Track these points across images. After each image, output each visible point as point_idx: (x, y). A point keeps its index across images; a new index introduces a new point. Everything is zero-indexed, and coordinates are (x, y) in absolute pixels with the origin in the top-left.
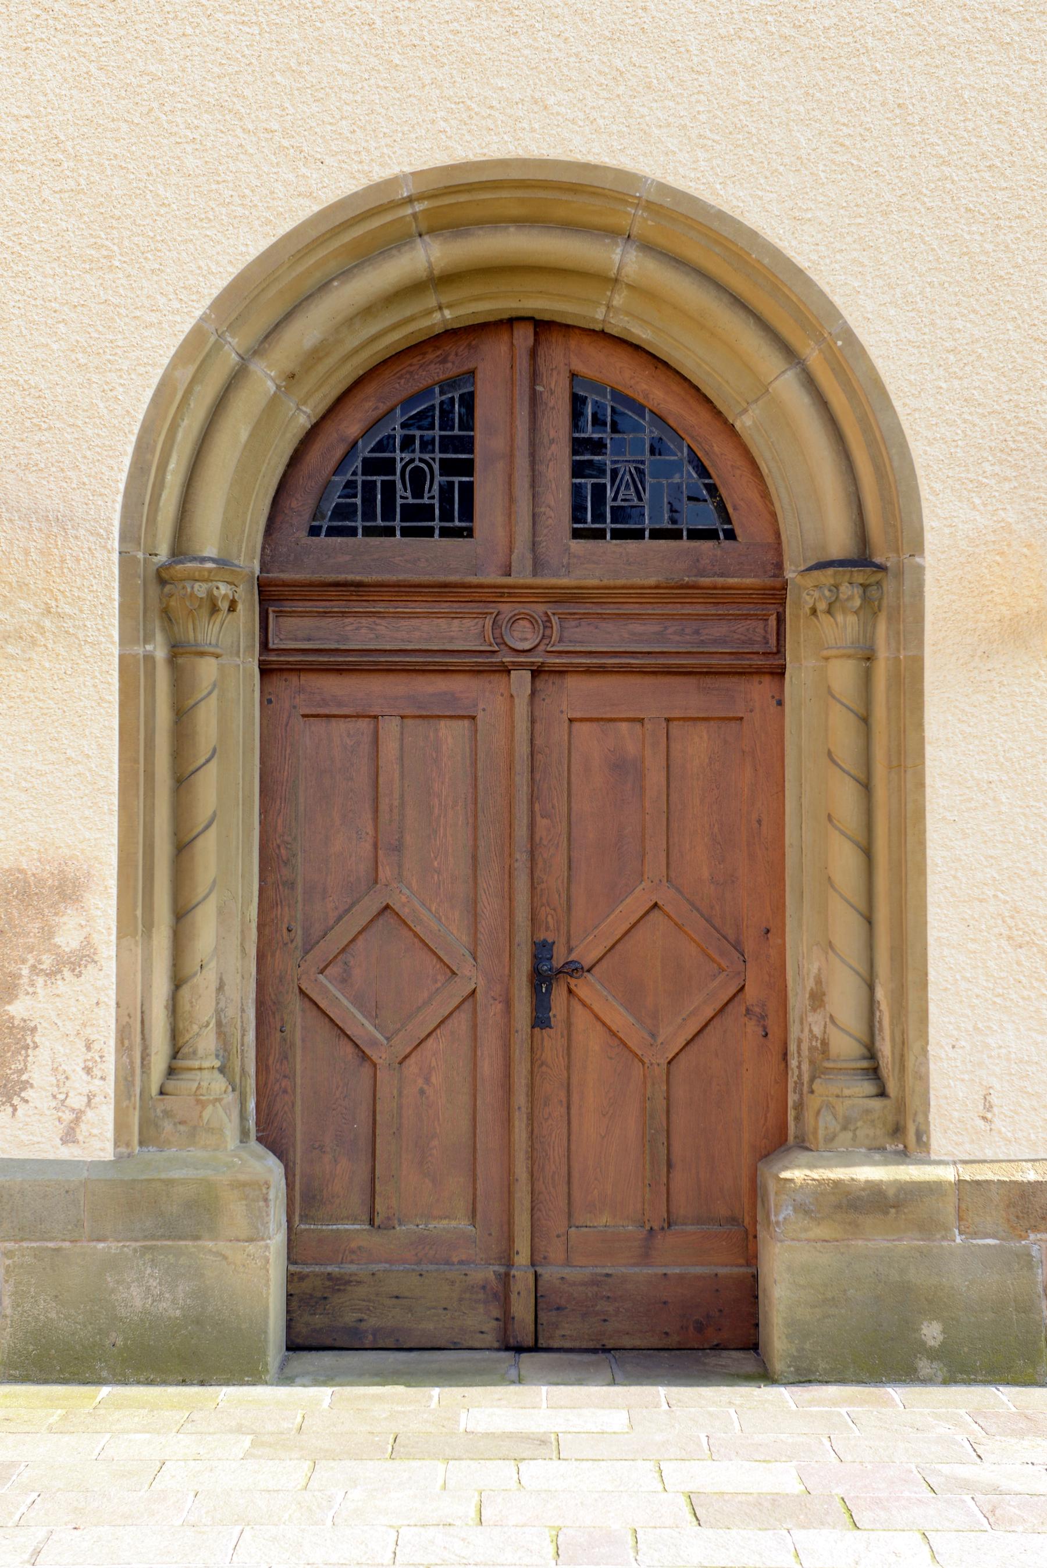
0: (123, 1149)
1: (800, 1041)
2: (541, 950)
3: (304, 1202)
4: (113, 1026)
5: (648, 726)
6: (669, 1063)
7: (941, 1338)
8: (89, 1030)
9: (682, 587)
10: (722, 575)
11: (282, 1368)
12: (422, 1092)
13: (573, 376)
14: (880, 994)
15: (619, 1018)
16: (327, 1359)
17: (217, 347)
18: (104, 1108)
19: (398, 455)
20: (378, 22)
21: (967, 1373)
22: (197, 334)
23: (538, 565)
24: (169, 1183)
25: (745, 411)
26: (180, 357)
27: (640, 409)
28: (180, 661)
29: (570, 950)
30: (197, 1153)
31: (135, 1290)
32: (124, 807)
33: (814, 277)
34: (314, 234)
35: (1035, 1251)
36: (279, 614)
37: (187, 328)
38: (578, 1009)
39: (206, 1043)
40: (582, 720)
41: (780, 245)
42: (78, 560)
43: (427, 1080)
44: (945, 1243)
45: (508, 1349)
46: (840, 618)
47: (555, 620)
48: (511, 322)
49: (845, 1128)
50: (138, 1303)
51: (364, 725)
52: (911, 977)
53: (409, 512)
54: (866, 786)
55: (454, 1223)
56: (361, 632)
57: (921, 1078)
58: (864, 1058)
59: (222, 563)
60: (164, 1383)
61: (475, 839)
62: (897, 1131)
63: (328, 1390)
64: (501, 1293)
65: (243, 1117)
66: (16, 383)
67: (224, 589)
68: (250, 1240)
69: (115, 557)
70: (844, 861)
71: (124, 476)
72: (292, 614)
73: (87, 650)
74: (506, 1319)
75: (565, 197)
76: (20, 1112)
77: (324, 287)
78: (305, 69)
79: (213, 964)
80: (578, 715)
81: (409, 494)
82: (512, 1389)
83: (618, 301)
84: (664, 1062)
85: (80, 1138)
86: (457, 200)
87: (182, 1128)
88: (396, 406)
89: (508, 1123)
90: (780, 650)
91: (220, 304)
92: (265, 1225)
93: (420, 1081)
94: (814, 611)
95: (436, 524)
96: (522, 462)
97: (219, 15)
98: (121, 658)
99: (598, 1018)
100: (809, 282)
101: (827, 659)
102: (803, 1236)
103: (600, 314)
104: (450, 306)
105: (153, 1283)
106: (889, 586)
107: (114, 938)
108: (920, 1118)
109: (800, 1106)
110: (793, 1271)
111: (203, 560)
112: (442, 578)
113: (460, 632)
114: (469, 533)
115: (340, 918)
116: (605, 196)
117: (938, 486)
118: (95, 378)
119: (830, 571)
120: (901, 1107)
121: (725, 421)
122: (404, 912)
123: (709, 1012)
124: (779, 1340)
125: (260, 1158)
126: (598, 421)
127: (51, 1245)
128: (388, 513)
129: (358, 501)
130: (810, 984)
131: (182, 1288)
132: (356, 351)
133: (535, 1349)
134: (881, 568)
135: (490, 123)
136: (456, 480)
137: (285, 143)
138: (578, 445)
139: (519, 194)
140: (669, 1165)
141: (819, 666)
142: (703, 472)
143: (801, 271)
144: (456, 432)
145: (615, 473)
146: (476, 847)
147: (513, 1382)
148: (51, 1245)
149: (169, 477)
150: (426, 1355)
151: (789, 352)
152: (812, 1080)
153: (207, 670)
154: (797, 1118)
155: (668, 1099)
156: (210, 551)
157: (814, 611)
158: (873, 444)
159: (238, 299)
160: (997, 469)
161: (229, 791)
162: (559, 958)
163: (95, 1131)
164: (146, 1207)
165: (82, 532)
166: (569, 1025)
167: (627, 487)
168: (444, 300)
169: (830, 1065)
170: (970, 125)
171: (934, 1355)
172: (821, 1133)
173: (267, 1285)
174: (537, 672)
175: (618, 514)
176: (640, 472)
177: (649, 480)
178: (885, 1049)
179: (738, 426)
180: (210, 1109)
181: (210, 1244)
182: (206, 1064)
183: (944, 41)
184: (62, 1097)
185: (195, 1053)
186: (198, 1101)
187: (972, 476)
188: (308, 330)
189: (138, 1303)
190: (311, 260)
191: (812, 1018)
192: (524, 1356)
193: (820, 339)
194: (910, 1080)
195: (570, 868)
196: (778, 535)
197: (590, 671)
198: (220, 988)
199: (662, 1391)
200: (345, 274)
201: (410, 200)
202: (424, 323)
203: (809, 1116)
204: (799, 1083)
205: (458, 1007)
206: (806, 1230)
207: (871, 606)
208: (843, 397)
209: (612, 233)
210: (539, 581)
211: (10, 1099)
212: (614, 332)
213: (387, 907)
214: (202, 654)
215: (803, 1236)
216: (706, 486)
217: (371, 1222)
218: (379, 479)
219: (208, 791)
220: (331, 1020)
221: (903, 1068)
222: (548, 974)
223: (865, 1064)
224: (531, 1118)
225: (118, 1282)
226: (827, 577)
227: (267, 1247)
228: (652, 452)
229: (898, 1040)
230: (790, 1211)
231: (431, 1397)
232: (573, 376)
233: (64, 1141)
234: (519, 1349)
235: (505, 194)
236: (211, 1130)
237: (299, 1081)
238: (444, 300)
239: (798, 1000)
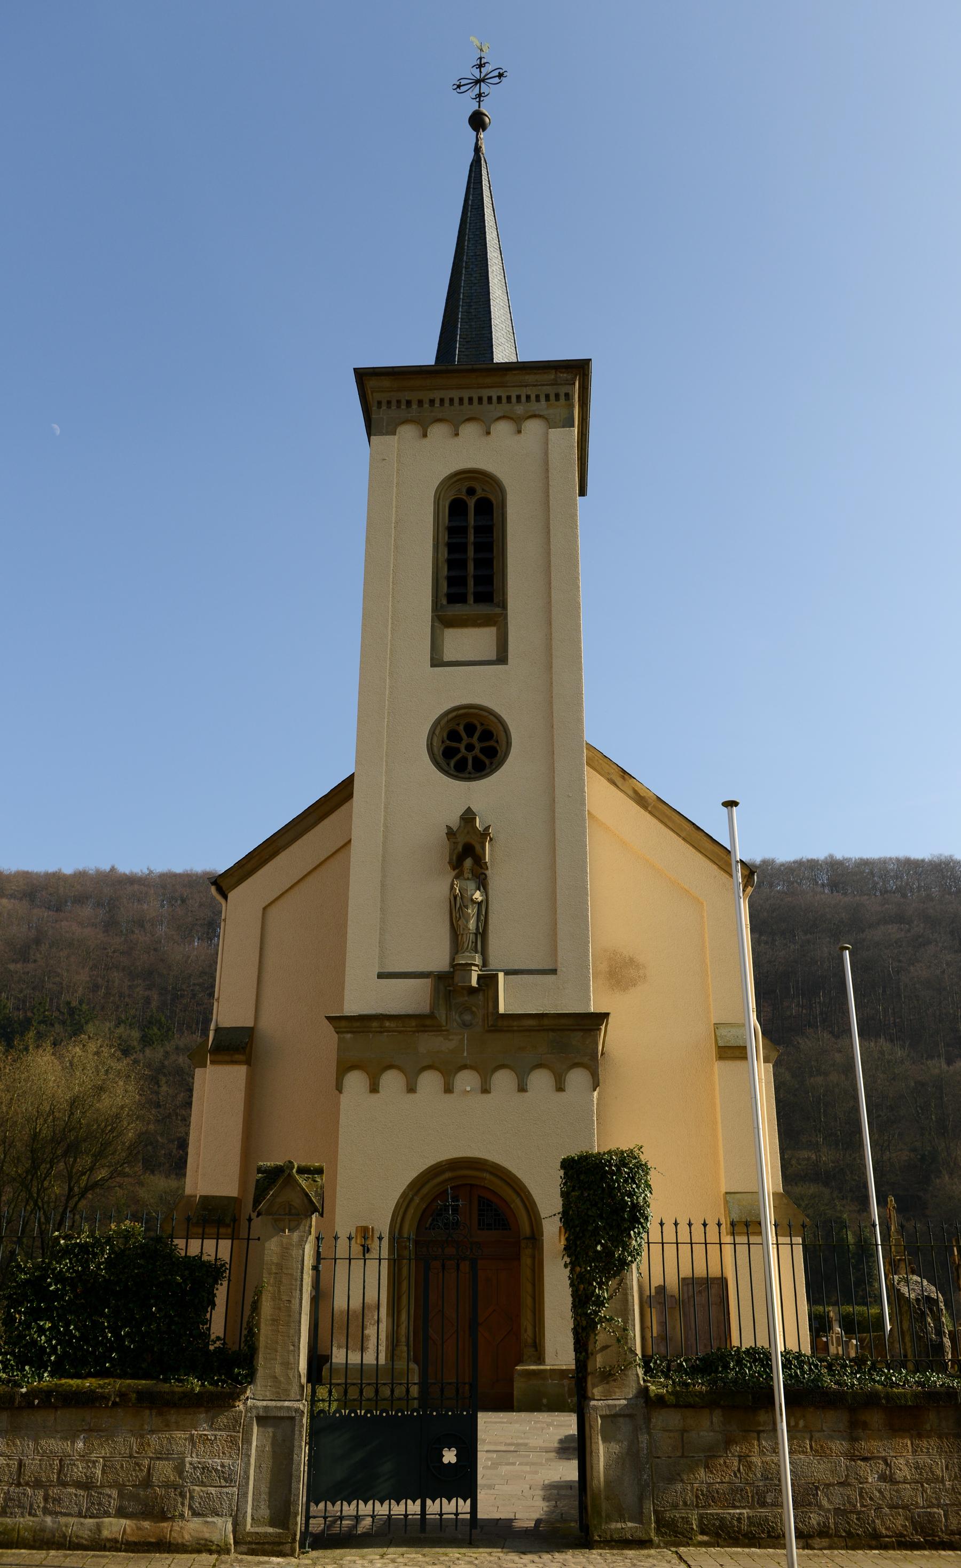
6: (265, 909)
22: (404, 1192)
54: (534, 1285)
62: (539, 1359)
70: (529, 1301)
110: (519, 1386)
141: (526, 1261)
188: (425, 1191)
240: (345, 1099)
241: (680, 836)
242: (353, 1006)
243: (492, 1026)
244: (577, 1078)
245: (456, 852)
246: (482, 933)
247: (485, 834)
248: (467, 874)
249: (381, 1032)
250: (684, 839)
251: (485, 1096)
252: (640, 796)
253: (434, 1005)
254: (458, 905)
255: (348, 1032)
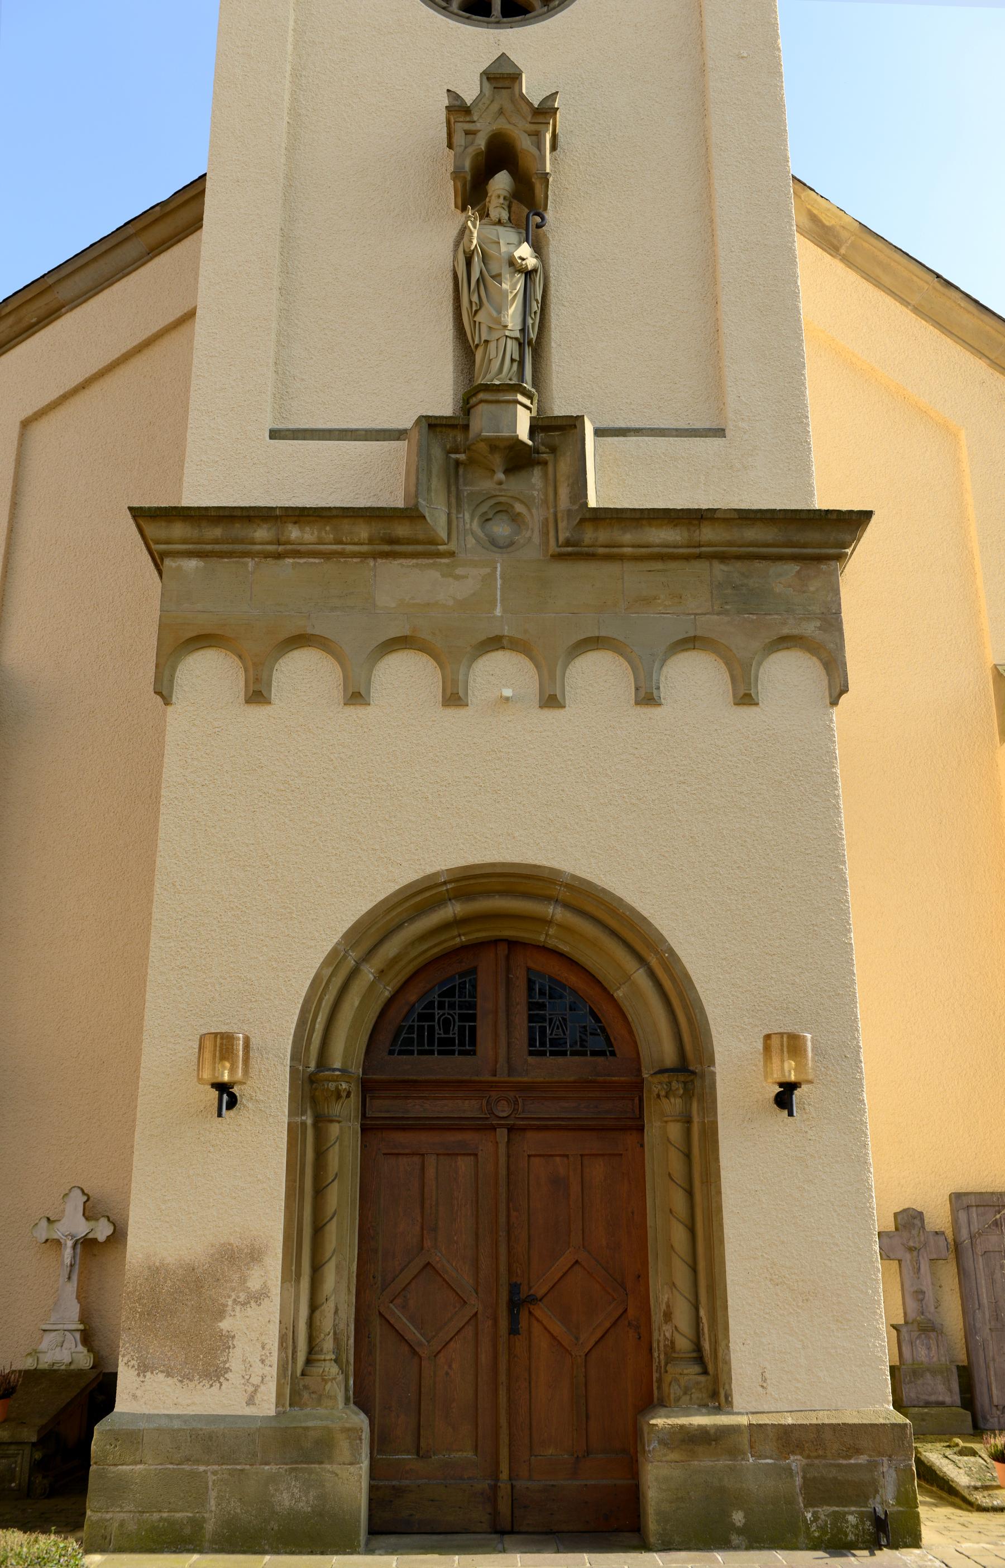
0: (280, 1409)
1: (659, 1342)
2: (514, 1288)
3: (381, 1441)
4: (277, 1335)
5: (571, 1159)
6: (26, 424)
7: (743, 1521)
8: (263, 1337)
9: (587, 1082)
10: (609, 1075)
11: (367, 1544)
12: (447, 1374)
13: (528, 969)
14: (702, 1313)
15: (557, 1328)
16: (392, 1539)
17: (345, 957)
18: (271, 1384)
19: (436, 1011)
20: (430, 797)
21: (759, 1542)
22: (334, 951)
23: (511, 1070)
24: (306, 1429)
25: (619, 988)
26: (326, 963)
27: (564, 987)
28: (320, 1125)
29: (530, 1288)
30: (321, 1411)
31: (285, 1495)
32: (288, 1207)
33: (652, 922)
34: (396, 900)
35: (794, 1466)
36: (372, 1098)
37: (329, 948)
38: (535, 1323)
39: (328, 1344)
40: (535, 1156)
41: (634, 905)
42: (268, 1071)
43: (450, 1367)
44: (743, 1462)
45: (496, 1532)
46: (672, 1100)
47: (520, 1100)
48: (496, 942)
49: (685, 1393)
50: (287, 1503)
51: (416, 1159)
52: (718, 1303)
53: (442, 1042)
54: (690, 1193)
55: (465, 1454)
56: (417, 1108)
57: (726, 1363)
58: (694, 1351)
59: (342, 1070)
60: (300, 1553)
61: (477, 1224)
62: (714, 1395)
63: (395, 1557)
64: (492, 1497)
65: (347, 1390)
66: (240, 978)
67: (344, 1086)
68: (351, 1464)
69: (288, 1069)
70: (679, 1235)
71: (294, 1026)
72: (379, 1098)
73: (271, 1120)
74: (495, 1513)
75: (524, 881)
76: (224, 1387)
77: (400, 926)
78: (393, 819)
79: (333, 1298)
80: (586, 1152)
81: (442, 1032)
82: (500, 1555)
83: (551, 932)
84: (583, 1354)
85: (257, 1402)
86: (469, 883)
87: (314, 1396)
88: (434, 987)
89: (496, 1391)
90: (641, 1117)
91: (347, 936)
92: (360, 1454)
93: (446, 1367)
94: (658, 1096)
95: (456, 1048)
96: (502, 1015)
97: (351, 794)
98: (289, 1124)
99: (546, 1328)
100: (650, 924)
101: (666, 1122)
102: (664, 1459)
103: (542, 938)
104: (464, 935)
105: (296, 1491)
106: (698, 1083)
107: (279, 1283)
108: (727, 1387)
109: (660, 1380)
110: (660, 1478)
111: (334, 1070)
112: (460, 1078)
113: (469, 1107)
114: (473, 1053)
115: (402, 1270)
116: (544, 880)
117: (721, 1030)
118: (281, 974)
119: (666, 1075)
120: (716, 1380)
121: (608, 993)
122: (438, 1266)
123: (608, 1325)
124: (652, 1525)
125: (357, 1414)
126: (542, 993)
127: (239, 1467)
128: (431, 1043)
129: (415, 1036)
130: (664, 1307)
131: (312, 1494)
132: (415, 958)
133: (512, 1532)
134: (693, 1073)
135: (486, 845)
136: (467, 1024)
137: (382, 855)
138: (531, 1006)
139: (501, 879)
140: (587, 1417)
141: (662, 1130)
142: (597, 1020)
143: (645, 918)
144: (467, 999)
145: (551, 1020)
146: (477, 1228)
147: (500, 1552)
148: (239, 1467)
149: (317, 1026)
150: (449, 1537)
151: (641, 960)
152: (666, 1364)
153: (334, 1129)
154: (659, 1388)
155: (585, 1377)
156: (337, 1065)
157: (658, 1096)
158: (685, 1007)
159: (355, 934)
160: (751, 1020)
161: (342, 1197)
162: (524, 1293)
163: (265, 1398)
164: (293, 1444)
165: (271, 1055)
166: (530, 1332)
167: (558, 1028)
168: (462, 931)
169: (676, 1355)
170: (727, 847)
171: (740, 1531)
172: (672, 1396)
173: (360, 1491)
174: (511, 1129)
175: (553, 1042)
176: (564, 1020)
177: (569, 1024)
178: (706, 1345)
179: (615, 995)
180: (330, 1384)
181: (328, 1467)
182: (328, 1357)
183: (712, 807)
184: (247, 1377)
185: (322, 1350)
186: (323, 1380)
187: (738, 1024)
188: (391, 948)
189: (287, 1503)
190: (394, 913)
191: (665, 1328)
192: (506, 1537)
193: (656, 952)
194: (720, 1365)
195: (529, 1241)
196: (638, 1054)
197: (539, 1128)
198: (336, 1312)
199: (586, 1556)
200: (411, 920)
201: (445, 883)
202: (452, 943)
203: (665, 1386)
204: (659, 1367)
205: (467, 1322)
206: (665, 1455)
207: (688, 1094)
208: (669, 982)
209: (548, 899)
210: (511, 1079)
211: (218, 1378)
212: (550, 947)
213: (429, 1263)
214: (332, 1121)
215: (664, 1459)
216: (600, 1027)
217: (418, 1454)
218: (426, 1024)
219: (333, 1198)
220: (397, 1331)
221: (716, 1357)
222: (518, 1303)
223: (694, 1355)
224: (509, 1390)
225: (276, 1490)
226: (664, 1078)
227: (361, 1468)
228: (571, 1009)
229: (713, 1340)
230: (656, 1444)
231: (454, 1561)
232: (528, 969)
233: (248, 1404)
234: (503, 1533)
235: (493, 880)
236: (329, 1397)
237: (378, 1367)
238: (462, 931)
239: (657, 1317)
240: (178, 718)
241: (905, 303)
242: (206, 484)
243: (568, 543)
244: (787, 674)
245: (471, 150)
246: (533, 344)
247: (545, 111)
248: (497, 210)
249: (278, 556)
250: (916, 310)
251: (551, 715)
252: (823, 226)
253: (418, 487)
254: (475, 275)
255: (190, 554)
